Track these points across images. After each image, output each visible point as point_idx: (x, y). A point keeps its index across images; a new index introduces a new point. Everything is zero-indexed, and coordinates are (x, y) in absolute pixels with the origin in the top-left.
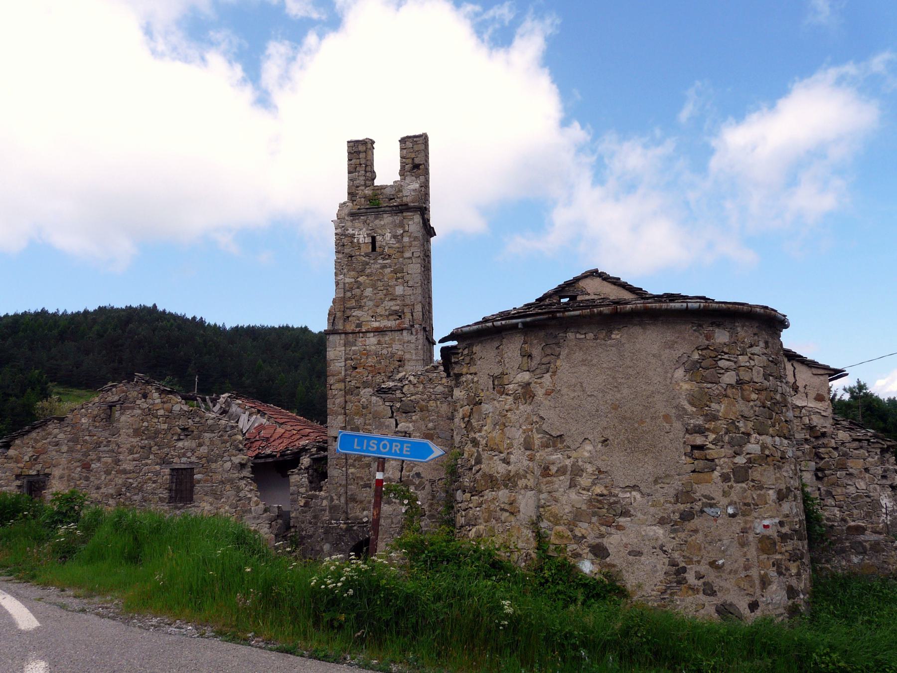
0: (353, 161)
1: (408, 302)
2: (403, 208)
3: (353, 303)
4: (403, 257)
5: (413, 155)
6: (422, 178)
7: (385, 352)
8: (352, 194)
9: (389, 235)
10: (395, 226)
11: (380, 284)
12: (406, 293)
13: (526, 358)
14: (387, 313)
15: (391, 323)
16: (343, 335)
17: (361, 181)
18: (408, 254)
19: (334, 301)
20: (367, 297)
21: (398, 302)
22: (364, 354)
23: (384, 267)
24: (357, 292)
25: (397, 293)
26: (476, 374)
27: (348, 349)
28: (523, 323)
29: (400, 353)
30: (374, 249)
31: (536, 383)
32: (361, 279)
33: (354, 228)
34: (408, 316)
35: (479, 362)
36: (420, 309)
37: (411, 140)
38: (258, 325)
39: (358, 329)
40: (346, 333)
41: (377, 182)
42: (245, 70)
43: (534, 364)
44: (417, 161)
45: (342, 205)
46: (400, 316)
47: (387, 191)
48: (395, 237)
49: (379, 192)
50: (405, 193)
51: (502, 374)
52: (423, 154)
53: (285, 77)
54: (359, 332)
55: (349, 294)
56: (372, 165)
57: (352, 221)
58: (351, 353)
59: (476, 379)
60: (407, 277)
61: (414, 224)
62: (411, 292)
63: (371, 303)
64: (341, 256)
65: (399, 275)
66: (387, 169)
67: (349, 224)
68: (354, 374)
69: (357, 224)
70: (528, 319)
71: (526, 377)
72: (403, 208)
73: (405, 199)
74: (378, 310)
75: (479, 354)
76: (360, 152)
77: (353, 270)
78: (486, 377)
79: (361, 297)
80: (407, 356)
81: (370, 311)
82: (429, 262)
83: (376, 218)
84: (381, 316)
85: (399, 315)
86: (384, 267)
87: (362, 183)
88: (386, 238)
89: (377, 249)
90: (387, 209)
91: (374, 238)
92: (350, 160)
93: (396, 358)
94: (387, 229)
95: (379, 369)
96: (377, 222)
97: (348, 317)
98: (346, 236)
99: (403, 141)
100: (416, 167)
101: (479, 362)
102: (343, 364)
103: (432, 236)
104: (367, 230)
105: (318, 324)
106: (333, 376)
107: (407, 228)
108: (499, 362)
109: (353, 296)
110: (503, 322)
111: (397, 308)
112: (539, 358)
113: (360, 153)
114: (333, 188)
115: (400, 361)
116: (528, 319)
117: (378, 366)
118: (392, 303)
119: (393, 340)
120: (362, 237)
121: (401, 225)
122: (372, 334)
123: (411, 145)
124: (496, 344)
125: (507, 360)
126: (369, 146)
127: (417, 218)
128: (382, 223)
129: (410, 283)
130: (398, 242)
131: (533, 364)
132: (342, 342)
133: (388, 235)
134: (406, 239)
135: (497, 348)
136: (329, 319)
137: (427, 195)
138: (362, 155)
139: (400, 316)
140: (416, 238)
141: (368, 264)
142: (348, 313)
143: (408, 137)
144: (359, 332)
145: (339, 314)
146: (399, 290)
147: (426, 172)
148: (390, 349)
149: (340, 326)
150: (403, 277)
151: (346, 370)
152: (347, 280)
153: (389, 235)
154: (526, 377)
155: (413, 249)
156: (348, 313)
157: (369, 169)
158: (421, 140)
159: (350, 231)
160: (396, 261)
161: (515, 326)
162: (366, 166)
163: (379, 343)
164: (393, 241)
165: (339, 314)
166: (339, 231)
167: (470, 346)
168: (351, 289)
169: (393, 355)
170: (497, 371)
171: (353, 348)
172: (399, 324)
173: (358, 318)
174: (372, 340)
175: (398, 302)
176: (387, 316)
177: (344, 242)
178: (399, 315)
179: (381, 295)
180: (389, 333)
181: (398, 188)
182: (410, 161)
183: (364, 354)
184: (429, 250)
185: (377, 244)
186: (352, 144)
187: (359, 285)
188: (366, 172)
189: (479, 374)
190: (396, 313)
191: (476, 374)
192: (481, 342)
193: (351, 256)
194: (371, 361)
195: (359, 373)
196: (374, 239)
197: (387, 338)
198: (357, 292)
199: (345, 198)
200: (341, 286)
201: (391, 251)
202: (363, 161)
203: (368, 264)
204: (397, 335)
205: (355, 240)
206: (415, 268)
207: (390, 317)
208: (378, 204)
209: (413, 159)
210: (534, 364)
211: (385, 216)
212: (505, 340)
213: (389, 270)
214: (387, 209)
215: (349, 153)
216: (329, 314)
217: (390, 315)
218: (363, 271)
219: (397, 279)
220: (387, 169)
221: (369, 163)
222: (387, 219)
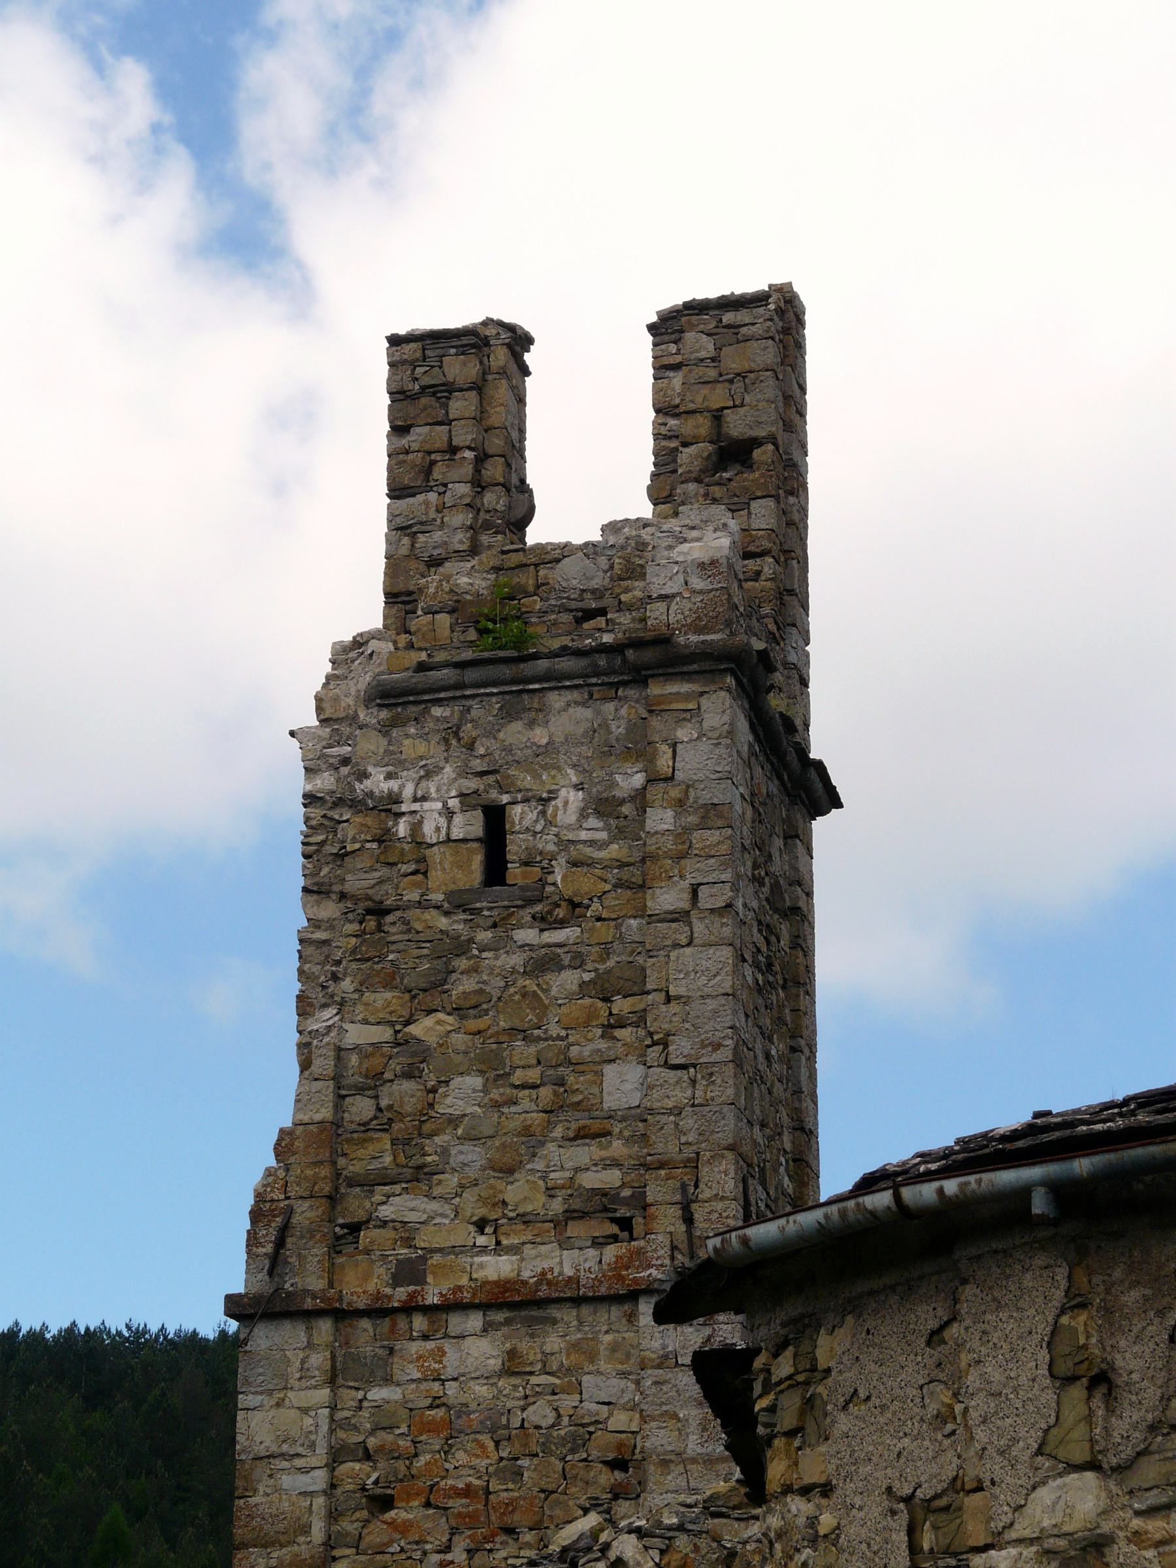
0: (419, 434)
1: (666, 1146)
2: (644, 661)
3: (380, 1154)
4: (641, 912)
5: (718, 397)
6: (763, 514)
7: (540, 1413)
8: (399, 597)
9: (575, 798)
10: (608, 751)
11: (521, 1051)
12: (657, 1100)
13: (1077, 1392)
14: (557, 1206)
15: (576, 1261)
16: (325, 1326)
17: (453, 533)
18: (668, 898)
19: (284, 1145)
20: (454, 1121)
21: (617, 1148)
22: (432, 1428)
23: (545, 963)
24: (403, 1093)
25: (610, 1103)
26: (826, 1489)
27: (349, 1397)
28: (1055, 1188)
29: (620, 1420)
30: (495, 871)
31: (1137, 1538)
32: (424, 1028)
33: (395, 764)
34: (668, 1221)
35: (843, 1423)
36: (730, 1186)
37: (708, 321)
38: (117, 1324)
39: (401, 1293)
40: (342, 1315)
41: (535, 535)
42: (163, 90)
43: (1126, 1425)
44: (737, 425)
45: (348, 654)
46: (625, 1224)
47: (570, 574)
48: (603, 806)
49: (527, 579)
50: (660, 580)
51: (956, 1485)
52: (769, 388)
53: (353, 126)
54: (410, 1308)
55: (361, 1108)
56: (515, 452)
57: (385, 729)
58: (365, 1420)
59: (827, 1521)
60: (664, 1017)
61: (704, 739)
62: (681, 1095)
63: (472, 1156)
64: (329, 910)
65: (621, 1005)
66: (589, 463)
67: (370, 744)
68: (376, 1533)
69: (413, 744)
70: (1082, 1166)
71: (1079, 1500)
72: (644, 661)
73: (657, 613)
74: (516, 1192)
75: (845, 1379)
76: (449, 389)
77: (389, 983)
78: (875, 1507)
79: (426, 1118)
80: (659, 1439)
81: (469, 1196)
82: (802, 944)
83: (509, 714)
84: (526, 1219)
85: (619, 1216)
86: (545, 963)
87: (460, 540)
88: (560, 816)
89: (514, 872)
90: (566, 664)
91: (495, 818)
92: (398, 429)
93: (601, 1446)
94: (562, 770)
95: (511, 1506)
96: (514, 733)
97: (355, 1229)
98: (356, 805)
99: (668, 327)
100: (733, 453)
101: (843, 1423)
102: (319, 1479)
103: (819, 810)
104: (464, 772)
105: (178, 1275)
106: (266, 1543)
107: (664, 762)
108: (943, 1417)
109: (385, 1120)
110: (951, 1186)
111: (611, 1178)
112: (1152, 1394)
113: (456, 396)
114: (331, 574)
115: (619, 1464)
116: (1082, 1166)
117: (503, 1491)
118: (583, 1154)
119: (586, 1351)
120: (437, 811)
121: (638, 748)
122: (475, 1321)
123: (707, 347)
124: (927, 1316)
125: (979, 1405)
126: (500, 357)
127: (720, 708)
128: (540, 736)
129: (681, 1049)
130: (619, 834)
131: (1120, 1427)
132: (318, 1360)
133: (570, 801)
134: (660, 819)
135: (935, 1337)
136: (252, 1240)
137: (788, 601)
138: (462, 405)
139: (625, 1224)
140: (711, 813)
141: (461, 947)
142: (355, 1205)
143: (695, 308)
144: (410, 1308)
145: (305, 1213)
146: (622, 1085)
147: (790, 482)
148: (567, 1402)
149: (308, 1277)
150: (640, 1018)
151: (333, 1515)
152: (356, 1034)
153: (575, 798)
154: (1079, 1500)
155: (694, 871)
156: (355, 1205)
157: (494, 470)
158: (757, 322)
159: (378, 783)
160: (605, 932)
161: (1011, 1211)
162: (482, 458)
163: (513, 1366)
164: (595, 829)
165: (305, 1213)
166: (325, 782)
167: (800, 1333)
168: (373, 1082)
169: (583, 1433)
170: (929, 1474)
171: (377, 1394)
172: (622, 1263)
173: (406, 1233)
174: (476, 1349)
175: (617, 1148)
176: (560, 1223)
177: (344, 833)
178: (619, 1216)
179: (526, 1110)
180: (568, 1315)
181: (624, 549)
182: (701, 426)
183: (432, 1428)
184: (802, 884)
185: (515, 846)
186: (410, 350)
187: (415, 1059)
188: (479, 485)
189: (846, 1490)
190: (601, 1204)
191: (826, 1489)
192: (854, 1307)
193: (379, 911)
194: (468, 1464)
195: (403, 1528)
196: (495, 821)
197: (553, 1342)
198: (403, 1093)
199: (366, 611)
200: (323, 1064)
201: (585, 884)
202: (464, 435)
203: (461, 947)
204: (605, 1326)
205: (402, 828)
206: (703, 973)
207: (575, 1229)
208: (520, 642)
209: (717, 416)
210: (1126, 1425)
211: (556, 700)
212: (969, 1291)
213: (567, 980)
214: (566, 664)
215: (398, 395)
216: (256, 1215)
217: (571, 1215)
218: (438, 984)
219: (612, 1025)
220: (589, 463)
221: (496, 443)
222: (567, 717)
